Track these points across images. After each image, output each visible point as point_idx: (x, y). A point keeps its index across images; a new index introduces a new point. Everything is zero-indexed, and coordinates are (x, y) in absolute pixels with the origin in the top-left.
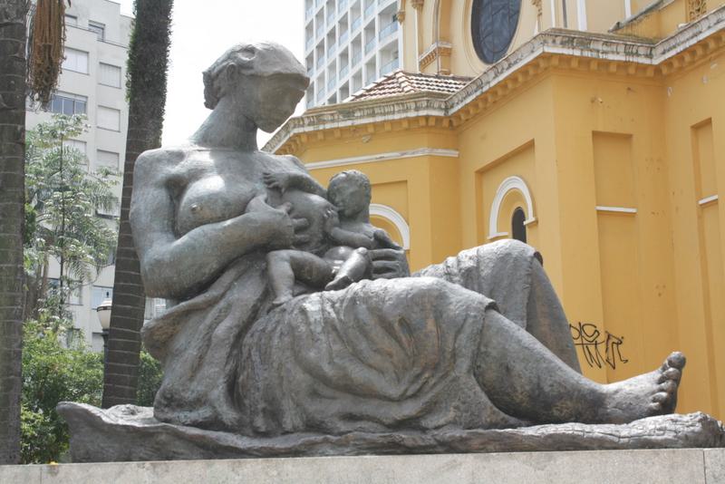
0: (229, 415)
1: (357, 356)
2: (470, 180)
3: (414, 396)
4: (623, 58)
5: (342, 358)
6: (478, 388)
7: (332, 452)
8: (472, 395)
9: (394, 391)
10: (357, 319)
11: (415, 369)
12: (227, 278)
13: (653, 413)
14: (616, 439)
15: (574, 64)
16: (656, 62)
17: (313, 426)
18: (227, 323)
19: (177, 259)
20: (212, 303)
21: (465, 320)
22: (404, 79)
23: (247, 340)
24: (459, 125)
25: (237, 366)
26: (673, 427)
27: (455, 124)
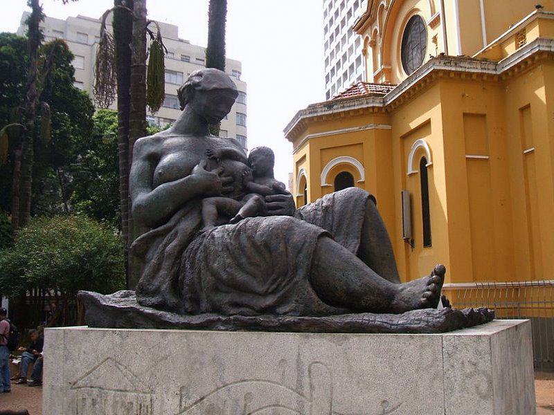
0: (172, 300)
1: (239, 266)
2: (397, 141)
3: (273, 292)
4: (480, 71)
5: (231, 268)
6: (310, 289)
7: (222, 328)
8: (306, 293)
9: (261, 289)
10: (240, 244)
11: (274, 275)
12: (176, 217)
13: (423, 306)
14: (389, 326)
15: (452, 75)
16: (498, 73)
17: (216, 309)
18: (173, 244)
19: (149, 204)
20: (170, 229)
21: (303, 245)
22: (362, 86)
23: (185, 254)
24: (391, 111)
25: (179, 270)
26: (426, 319)
27: (389, 111)
